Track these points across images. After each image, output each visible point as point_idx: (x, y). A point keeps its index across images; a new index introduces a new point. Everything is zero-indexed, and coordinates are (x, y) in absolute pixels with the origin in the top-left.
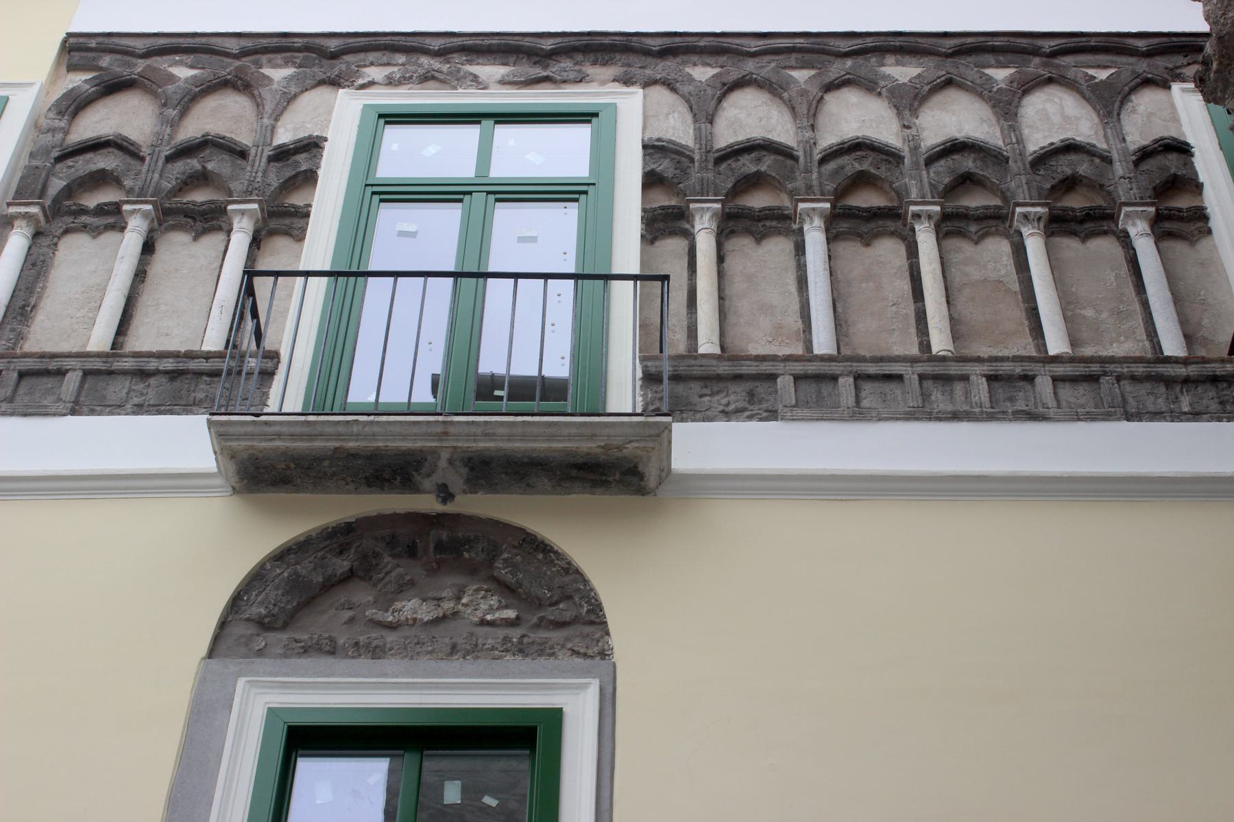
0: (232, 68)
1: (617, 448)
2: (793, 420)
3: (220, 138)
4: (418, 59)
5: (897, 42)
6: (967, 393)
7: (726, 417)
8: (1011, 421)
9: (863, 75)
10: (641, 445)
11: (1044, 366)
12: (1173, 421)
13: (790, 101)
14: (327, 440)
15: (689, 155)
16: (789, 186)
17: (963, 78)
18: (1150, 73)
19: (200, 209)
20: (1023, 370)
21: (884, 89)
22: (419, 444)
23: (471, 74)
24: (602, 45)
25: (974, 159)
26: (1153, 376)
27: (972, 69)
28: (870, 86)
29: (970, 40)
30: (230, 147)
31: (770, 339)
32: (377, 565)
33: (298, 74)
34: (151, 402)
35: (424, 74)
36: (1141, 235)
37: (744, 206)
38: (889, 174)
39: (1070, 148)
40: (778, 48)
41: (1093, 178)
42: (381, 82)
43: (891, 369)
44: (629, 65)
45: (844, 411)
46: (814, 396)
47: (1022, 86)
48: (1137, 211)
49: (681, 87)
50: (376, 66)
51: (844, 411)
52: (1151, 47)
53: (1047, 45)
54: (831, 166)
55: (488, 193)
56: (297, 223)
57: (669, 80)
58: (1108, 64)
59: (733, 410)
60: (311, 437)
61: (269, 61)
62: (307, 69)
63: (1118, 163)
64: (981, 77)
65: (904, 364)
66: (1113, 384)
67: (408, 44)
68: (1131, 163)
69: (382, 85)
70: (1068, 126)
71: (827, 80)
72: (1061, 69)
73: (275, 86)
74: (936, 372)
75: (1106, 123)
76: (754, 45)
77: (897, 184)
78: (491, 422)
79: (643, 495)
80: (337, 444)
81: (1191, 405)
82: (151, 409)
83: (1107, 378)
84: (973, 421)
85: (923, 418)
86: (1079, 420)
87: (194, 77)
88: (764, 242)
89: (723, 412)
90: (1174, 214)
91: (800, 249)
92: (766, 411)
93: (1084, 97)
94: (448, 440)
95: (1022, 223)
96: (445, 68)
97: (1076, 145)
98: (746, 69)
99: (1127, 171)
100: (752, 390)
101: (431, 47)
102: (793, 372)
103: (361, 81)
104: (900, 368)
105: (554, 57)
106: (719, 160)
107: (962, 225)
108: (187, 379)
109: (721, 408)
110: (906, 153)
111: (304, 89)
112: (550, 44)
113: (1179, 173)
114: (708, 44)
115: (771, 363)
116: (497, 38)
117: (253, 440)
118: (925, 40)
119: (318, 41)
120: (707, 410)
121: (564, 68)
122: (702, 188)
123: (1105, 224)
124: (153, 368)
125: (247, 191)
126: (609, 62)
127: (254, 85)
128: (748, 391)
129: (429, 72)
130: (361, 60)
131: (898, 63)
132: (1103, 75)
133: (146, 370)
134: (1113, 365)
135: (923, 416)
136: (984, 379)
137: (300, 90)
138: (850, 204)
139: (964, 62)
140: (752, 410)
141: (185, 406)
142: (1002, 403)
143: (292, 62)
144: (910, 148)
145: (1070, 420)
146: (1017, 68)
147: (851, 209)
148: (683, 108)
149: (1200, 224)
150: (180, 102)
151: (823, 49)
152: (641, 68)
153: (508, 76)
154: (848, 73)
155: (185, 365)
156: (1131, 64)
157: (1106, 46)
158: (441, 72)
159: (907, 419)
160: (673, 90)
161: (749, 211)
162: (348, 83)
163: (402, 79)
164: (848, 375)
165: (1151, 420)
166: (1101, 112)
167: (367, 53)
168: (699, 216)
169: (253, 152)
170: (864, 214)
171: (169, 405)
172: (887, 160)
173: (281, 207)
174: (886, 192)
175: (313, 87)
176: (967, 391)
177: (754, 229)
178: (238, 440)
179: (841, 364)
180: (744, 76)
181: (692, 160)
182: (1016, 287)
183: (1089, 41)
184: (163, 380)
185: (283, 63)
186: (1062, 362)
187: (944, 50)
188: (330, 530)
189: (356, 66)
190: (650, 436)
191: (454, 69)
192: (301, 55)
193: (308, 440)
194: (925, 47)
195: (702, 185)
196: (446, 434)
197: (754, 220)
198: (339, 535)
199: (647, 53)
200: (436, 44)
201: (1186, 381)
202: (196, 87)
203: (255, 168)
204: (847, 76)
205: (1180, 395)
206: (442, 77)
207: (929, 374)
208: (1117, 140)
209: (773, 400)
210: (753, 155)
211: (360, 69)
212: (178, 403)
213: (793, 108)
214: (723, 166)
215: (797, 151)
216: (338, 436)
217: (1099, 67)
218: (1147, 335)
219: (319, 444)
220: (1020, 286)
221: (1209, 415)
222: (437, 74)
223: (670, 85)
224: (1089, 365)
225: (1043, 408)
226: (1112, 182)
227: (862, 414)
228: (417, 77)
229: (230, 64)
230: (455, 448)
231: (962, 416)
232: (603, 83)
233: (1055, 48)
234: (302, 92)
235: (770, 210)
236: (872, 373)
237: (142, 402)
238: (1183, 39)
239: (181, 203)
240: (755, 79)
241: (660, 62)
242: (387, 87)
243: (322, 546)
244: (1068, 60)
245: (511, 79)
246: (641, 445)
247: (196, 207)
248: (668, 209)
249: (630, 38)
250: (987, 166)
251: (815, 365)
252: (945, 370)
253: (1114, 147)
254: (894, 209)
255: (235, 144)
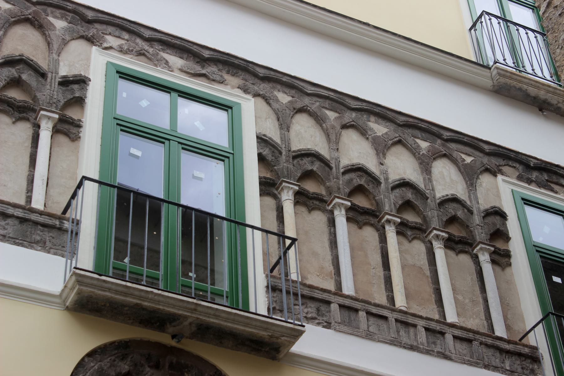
0: (31, 11)
1: (276, 338)
2: (340, 331)
3: (30, 60)
4: (135, 39)
5: (377, 110)
6: (415, 335)
7: (307, 320)
8: (436, 356)
9: (360, 124)
10: (288, 339)
11: (449, 329)
12: (502, 374)
13: (327, 130)
14: (134, 298)
15: (280, 150)
16: (327, 183)
17: (407, 142)
18: (489, 166)
19: (18, 104)
20: (441, 329)
21: (370, 136)
22: (180, 312)
23: (164, 59)
24: (234, 63)
25: (412, 192)
26: (495, 346)
27: (411, 138)
28: (363, 132)
29: (411, 120)
30: (36, 68)
31: (318, 274)
32: (143, 371)
33: (70, 28)
34: (11, 235)
35: (139, 51)
36: (487, 262)
37: (305, 189)
38: (374, 190)
39: (454, 200)
40: (321, 94)
41: (464, 220)
42: (116, 48)
43: (383, 312)
44: (246, 80)
45: (362, 332)
46: (347, 319)
47: (433, 155)
48: (486, 248)
49: (272, 103)
50: (112, 36)
51: (362, 332)
52: (491, 151)
53: (446, 134)
54: (347, 177)
55: (179, 143)
56: (74, 130)
57: (266, 96)
58: (471, 154)
59: (310, 317)
60: (125, 294)
61: (52, 13)
62: (74, 26)
63: (476, 216)
64: (415, 144)
65: (388, 311)
66: (479, 347)
67: (132, 28)
68: (482, 218)
69: (116, 50)
70: (453, 186)
71: (344, 123)
72: (450, 150)
73: (57, 32)
74: (403, 320)
75: (471, 190)
76: (310, 89)
77: (378, 198)
78: (220, 309)
79: (273, 360)
80: (139, 302)
81: (510, 366)
82: (11, 240)
83: (476, 342)
84: (420, 352)
85: (398, 345)
86: (465, 363)
87: (9, 10)
88: (313, 212)
89: (305, 317)
90: (497, 251)
91: (332, 223)
92: (326, 322)
93: (460, 170)
94: (195, 314)
95: (434, 239)
96: (151, 50)
97: (458, 199)
98: (305, 102)
99: (480, 222)
100: (318, 307)
101: (144, 35)
102: (339, 303)
103: (105, 45)
104: (387, 313)
105: (207, 62)
106: (294, 158)
107: (404, 229)
108: (29, 225)
109: (305, 315)
110: (382, 180)
111: (72, 39)
112: (207, 54)
113: (501, 229)
114: (287, 81)
115: (328, 294)
116: (179, 40)
117: (95, 288)
118: (390, 113)
119: (81, 9)
120: (298, 314)
121: (214, 71)
122: (288, 174)
123: (466, 247)
124: (11, 213)
125: (49, 103)
126: (236, 75)
127: (45, 27)
128: (317, 308)
129: (142, 50)
130: (105, 30)
131: (376, 122)
132: (469, 160)
133: (7, 213)
134: (478, 336)
135: (398, 344)
136: (424, 329)
137: (71, 38)
138: (355, 203)
139: (406, 131)
140: (319, 320)
141: (30, 242)
142: (431, 345)
143: (65, 17)
144: (384, 178)
145: (461, 363)
146: (431, 143)
147: (354, 206)
148: (273, 117)
149: (507, 259)
150: (4, 26)
151: (343, 103)
152: (253, 84)
153: (185, 67)
154: (353, 121)
155: (29, 216)
156: (480, 157)
157: (471, 143)
158: (148, 52)
159: (391, 344)
160: (269, 104)
161: (307, 193)
162: (98, 43)
163: (128, 51)
164: (363, 311)
165: (493, 371)
166: (468, 182)
167: (108, 26)
168: (287, 191)
169: (49, 75)
170: (361, 211)
171: (21, 240)
172: (372, 181)
173: (65, 117)
174: (371, 200)
175: (77, 38)
176: (415, 333)
177: (308, 203)
178: (86, 286)
179: (360, 303)
180: (304, 107)
181: (281, 153)
182: (428, 273)
183: (463, 138)
184: (16, 222)
185: (60, 16)
186: (457, 328)
187: (399, 122)
188: (117, 344)
189: (102, 33)
190: (294, 336)
191: (155, 52)
192: (71, 15)
193: (123, 296)
194: (390, 118)
195: (288, 171)
196: (195, 310)
197: (309, 199)
198: (122, 348)
199: (255, 75)
200: (147, 34)
201: (508, 352)
202: (12, 18)
203: (53, 88)
204: (353, 123)
205: (505, 359)
206: (150, 57)
207: (399, 320)
208: (475, 202)
209: (328, 316)
210: (309, 158)
211: (104, 36)
212: (26, 240)
213: (329, 136)
214: (295, 161)
215: (331, 163)
216: (140, 298)
217: (466, 154)
218: (485, 318)
219: (129, 299)
220: (431, 274)
221: (517, 374)
222: (146, 53)
223: (267, 100)
224: (468, 333)
225: (450, 353)
226: (473, 226)
227: (371, 336)
228: (135, 51)
229: (30, 8)
230: (198, 318)
231: (415, 348)
232: (233, 87)
233: (449, 137)
234: (71, 40)
235: (317, 195)
236: (374, 312)
237: (5, 234)
238: (504, 151)
239: (7, 97)
240: (309, 110)
241: (262, 83)
242: (119, 53)
243: (113, 353)
244: (453, 146)
245: (186, 69)
246: (288, 339)
247: (16, 103)
248: (268, 179)
249: (248, 64)
250: (418, 199)
251: (348, 301)
252: (407, 319)
253: (474, 205)
254: (374, 212)
255: (39, 67)
